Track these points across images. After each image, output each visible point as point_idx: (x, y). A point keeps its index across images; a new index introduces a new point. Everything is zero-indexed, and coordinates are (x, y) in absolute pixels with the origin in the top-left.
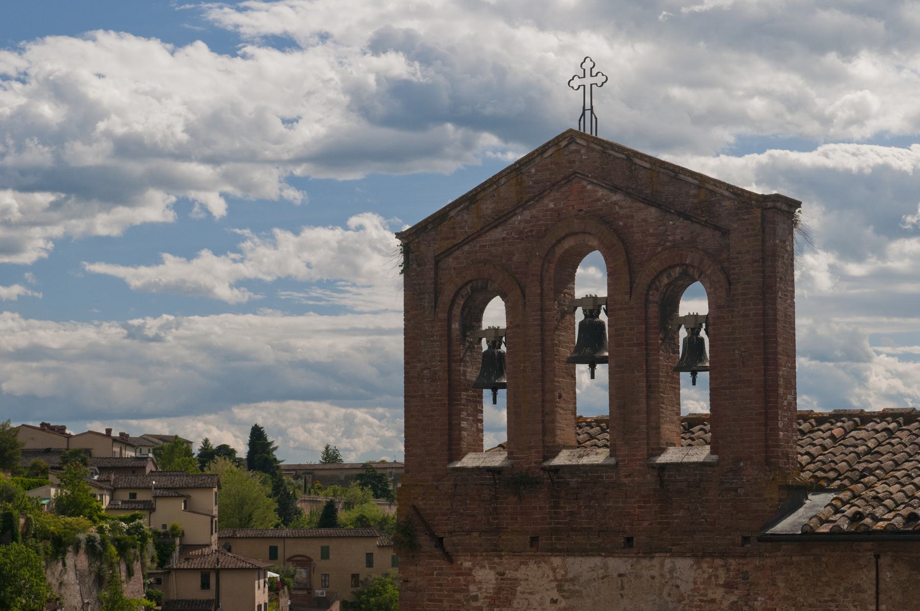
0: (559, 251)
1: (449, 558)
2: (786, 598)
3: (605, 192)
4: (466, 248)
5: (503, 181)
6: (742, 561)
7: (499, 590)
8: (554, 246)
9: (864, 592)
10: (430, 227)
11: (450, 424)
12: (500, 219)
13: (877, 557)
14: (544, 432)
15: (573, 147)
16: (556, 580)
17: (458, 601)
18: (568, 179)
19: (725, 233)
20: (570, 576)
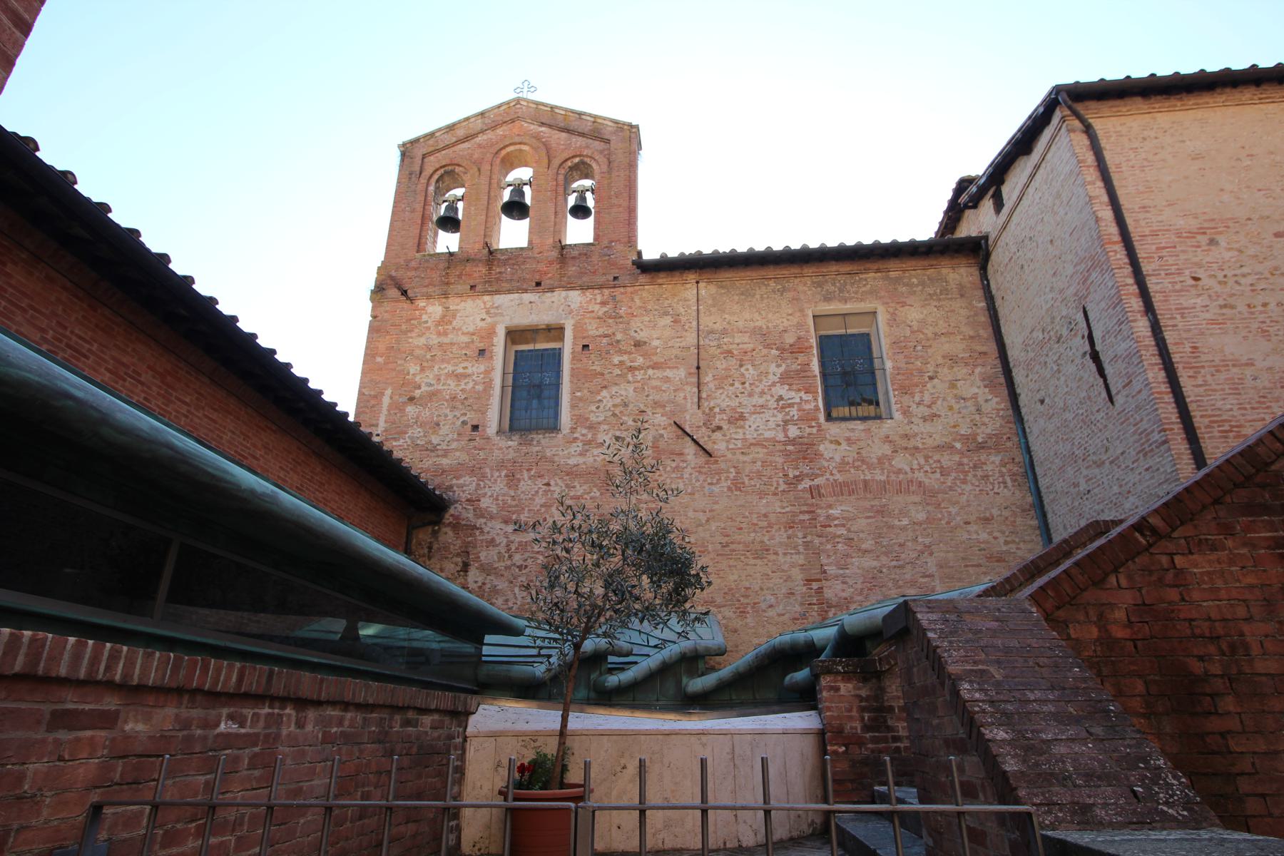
0: (504, 152)
1: (411, 300)
2: (640, 307)
3: (536, 127)
4: (444, 152)
5: (472, 120)
6: (612, 290)
7: (444, 316)
8: (501, 149)
9: (689, 300)
10: (422, 140)
11: (420, 235)
12: (467, 139)
13: (697, 282)
14: (485, 236)
15: (518, 106)
16: (485, 308)
17: (413, 325)
18: (513, 121)
19: (608, 141)
20: (496, 305)
